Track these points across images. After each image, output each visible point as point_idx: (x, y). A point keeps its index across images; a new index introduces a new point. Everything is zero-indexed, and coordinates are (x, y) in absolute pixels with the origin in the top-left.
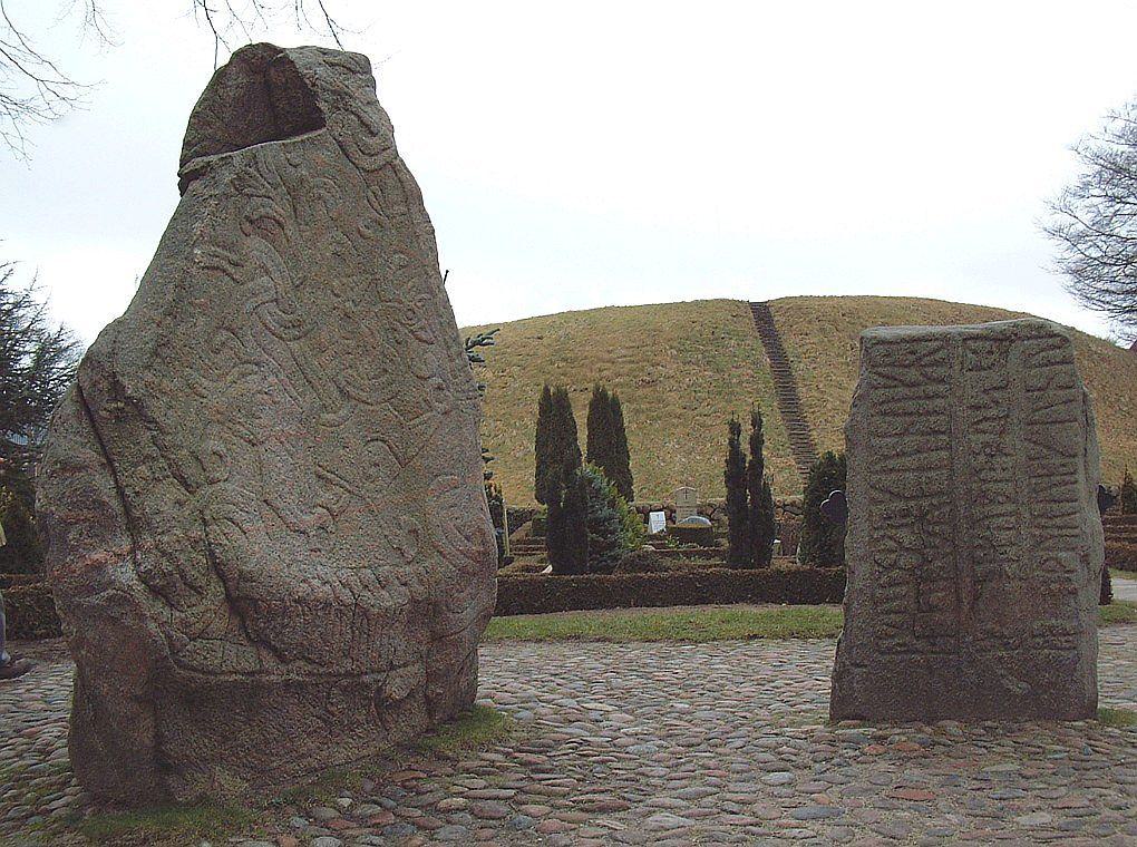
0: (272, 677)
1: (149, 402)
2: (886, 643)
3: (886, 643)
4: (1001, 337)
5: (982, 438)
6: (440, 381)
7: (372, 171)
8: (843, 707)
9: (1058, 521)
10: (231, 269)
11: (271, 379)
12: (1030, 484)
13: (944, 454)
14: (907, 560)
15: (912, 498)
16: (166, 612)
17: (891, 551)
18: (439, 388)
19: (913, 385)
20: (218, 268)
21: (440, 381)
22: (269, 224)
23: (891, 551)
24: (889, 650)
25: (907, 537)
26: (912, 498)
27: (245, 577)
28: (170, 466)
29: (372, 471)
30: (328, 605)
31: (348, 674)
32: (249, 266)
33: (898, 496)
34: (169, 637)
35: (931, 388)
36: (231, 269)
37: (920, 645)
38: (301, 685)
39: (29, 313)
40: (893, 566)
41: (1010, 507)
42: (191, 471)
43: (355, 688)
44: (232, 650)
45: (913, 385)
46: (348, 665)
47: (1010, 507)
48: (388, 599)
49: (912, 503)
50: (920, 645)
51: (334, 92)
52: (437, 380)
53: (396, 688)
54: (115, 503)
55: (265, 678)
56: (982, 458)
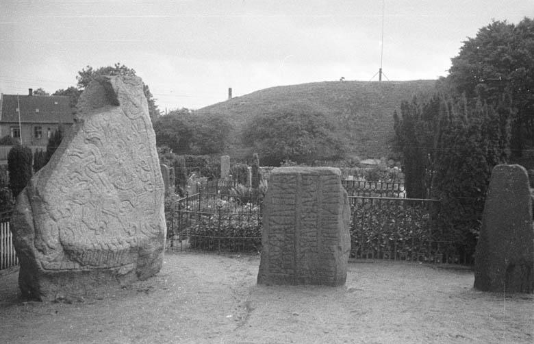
8: (260, 279)
10: (79, 155)
11: (91, 185)
15: (282, 224)
16: (42, 255)
22: (95, 139)
29: (123, 210)
30: (98, 251)
31: (105, 268)
32: (86, 153)
33: (278, 224)
35: (290, 190)
36: (79, 155)
37: (282, 271)
38: (89, 271)
43: (108, 271)
44: (64, 263)
46: (105, 266)
49: (282, 226)
50: (282, 271)
51: (124, 94)
53: (123, 271)
54: (32, 225)
55: (75, 271)
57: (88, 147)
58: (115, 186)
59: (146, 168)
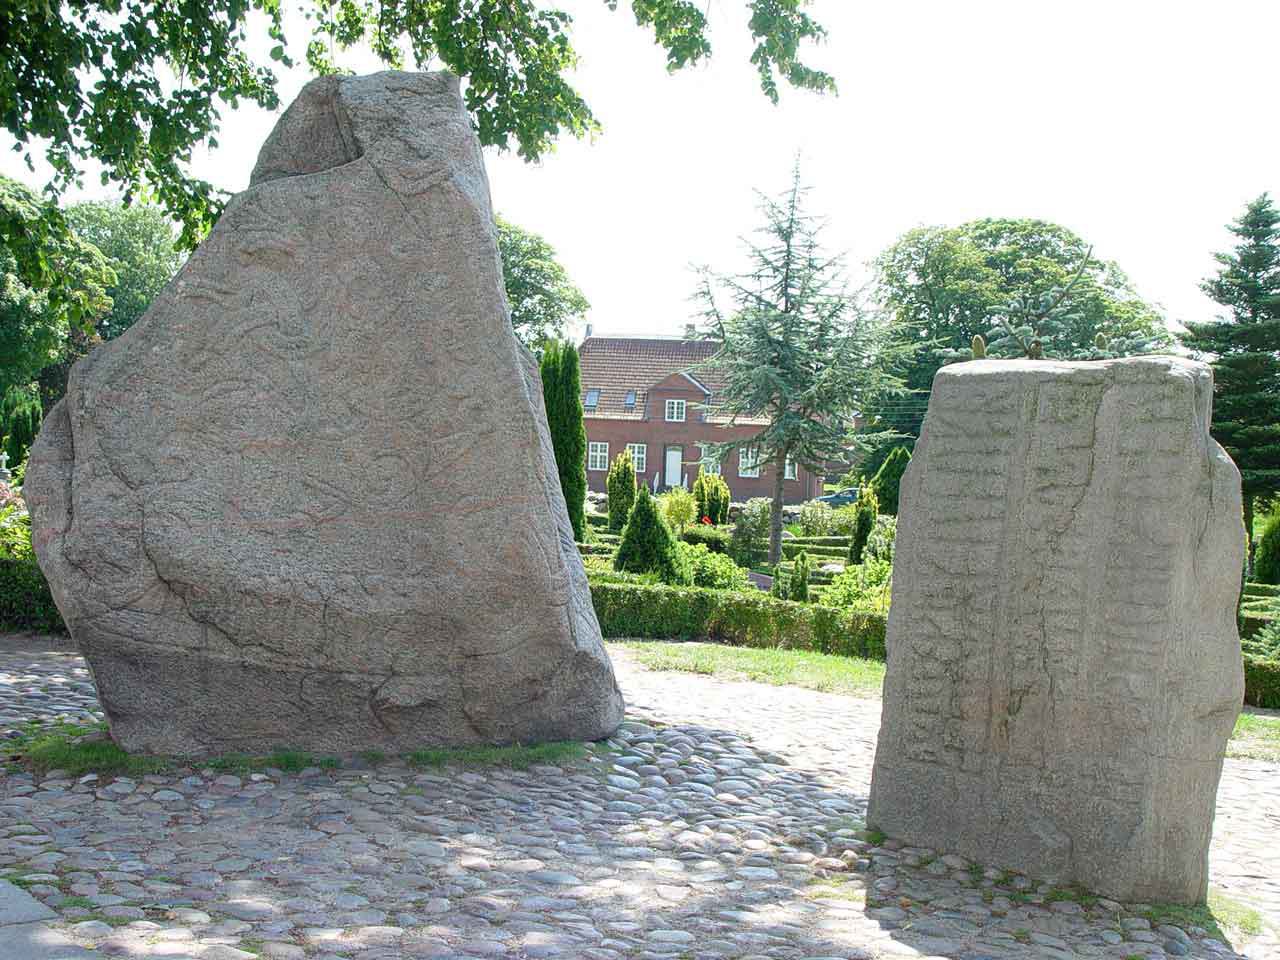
0: (222, 656)
1: (102, 412)
2: (912, 749)
3: (912, 749)
4: (1089, 380)
5: (1045, 510)
6: (480, 401)
7: (415, 195)
9: (1134, 631)
12: (1106, 576)
13: (997, 526)
14: (945, 651)
17: (929, 637)
18: (477, 408)
19: (977, 435)
20: (201, 297)
21: (480, 401)
23: (929, 637)
24: (915, 758)
25: (946, 621)
26: (959, 575)
27: (181, 565)
28: (112, 465)
30: (282, 601)
32: (242, 294)
34: (81, 602)
39: (847, 316)
40: (929, 655)
41: (1075, 604)
42: (135, 472)
45: (977, 435)
47: (1075, 604)
48: (383, 605)
52: (471, 402)
56: (1041, 537)
57: (258, 274)
58: (351, 408)
59: (462, 356)
